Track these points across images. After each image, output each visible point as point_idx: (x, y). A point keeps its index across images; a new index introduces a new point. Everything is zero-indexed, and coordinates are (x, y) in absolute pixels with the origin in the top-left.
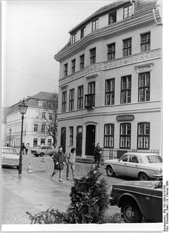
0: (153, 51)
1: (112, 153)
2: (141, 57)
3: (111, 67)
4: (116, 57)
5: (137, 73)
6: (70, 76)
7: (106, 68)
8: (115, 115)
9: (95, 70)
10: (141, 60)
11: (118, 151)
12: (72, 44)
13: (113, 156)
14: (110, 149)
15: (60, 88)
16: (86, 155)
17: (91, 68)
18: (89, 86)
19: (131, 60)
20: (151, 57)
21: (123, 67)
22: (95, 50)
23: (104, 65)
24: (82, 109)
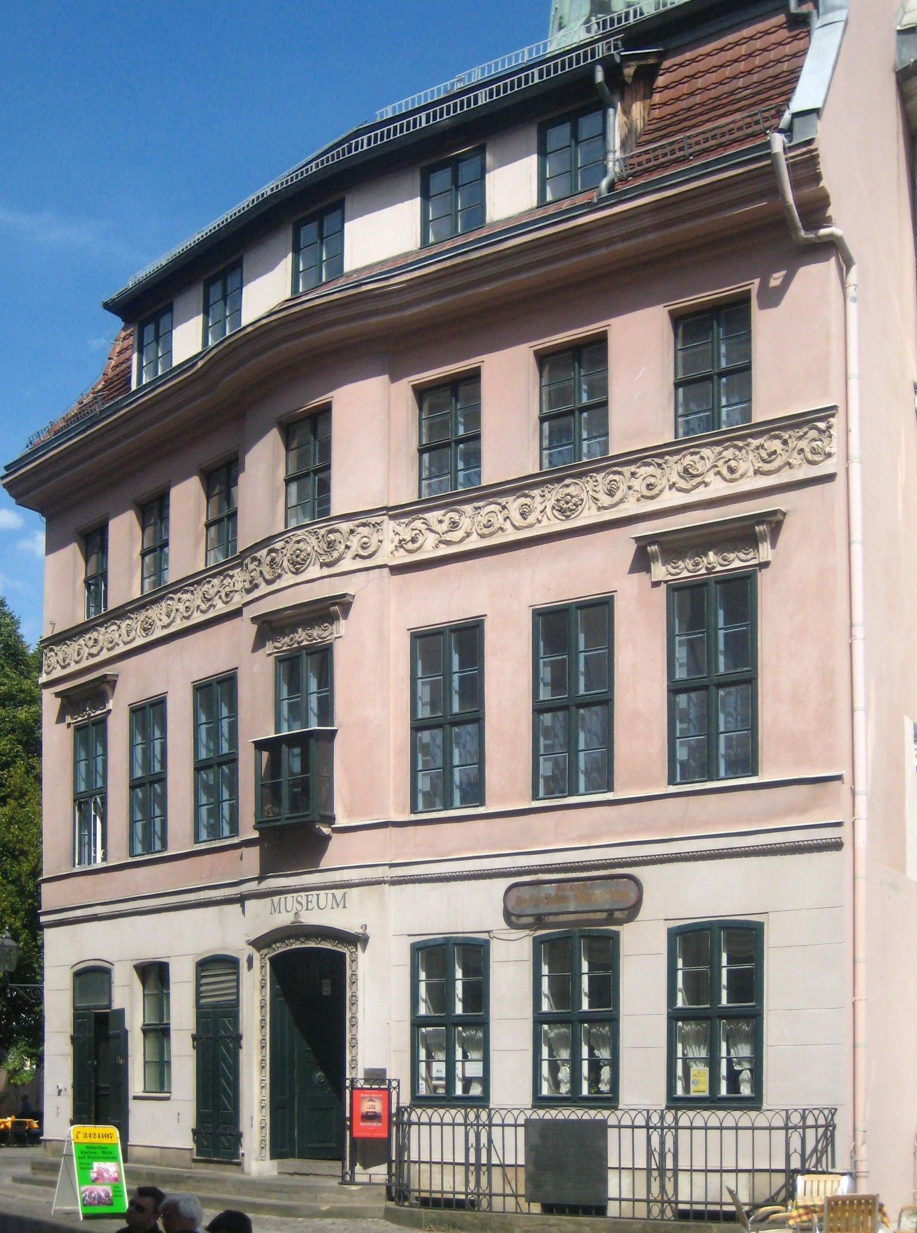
0: (774, 427)
1: (484, 1140)
2: (686, 470)
3: (448, 543)
4: (490, 474)
5: (656, 584)
6: (121, 613)
7: (410, 552)
8: (854, 889)
9: (323, 565)
10: (680, 490)
11: (528, 1123)
12: (134, 387)
13: (495, 1161)
14: (472, 1116)
15: (57, 695)
16: (274, 1156)
17: (291, 547)
18: (77, 814)
19: (611, 493)
20: (757, 472)
21: (844, 364)
22: (320, 427)
23: (399, 529)
24: (236, 840)
